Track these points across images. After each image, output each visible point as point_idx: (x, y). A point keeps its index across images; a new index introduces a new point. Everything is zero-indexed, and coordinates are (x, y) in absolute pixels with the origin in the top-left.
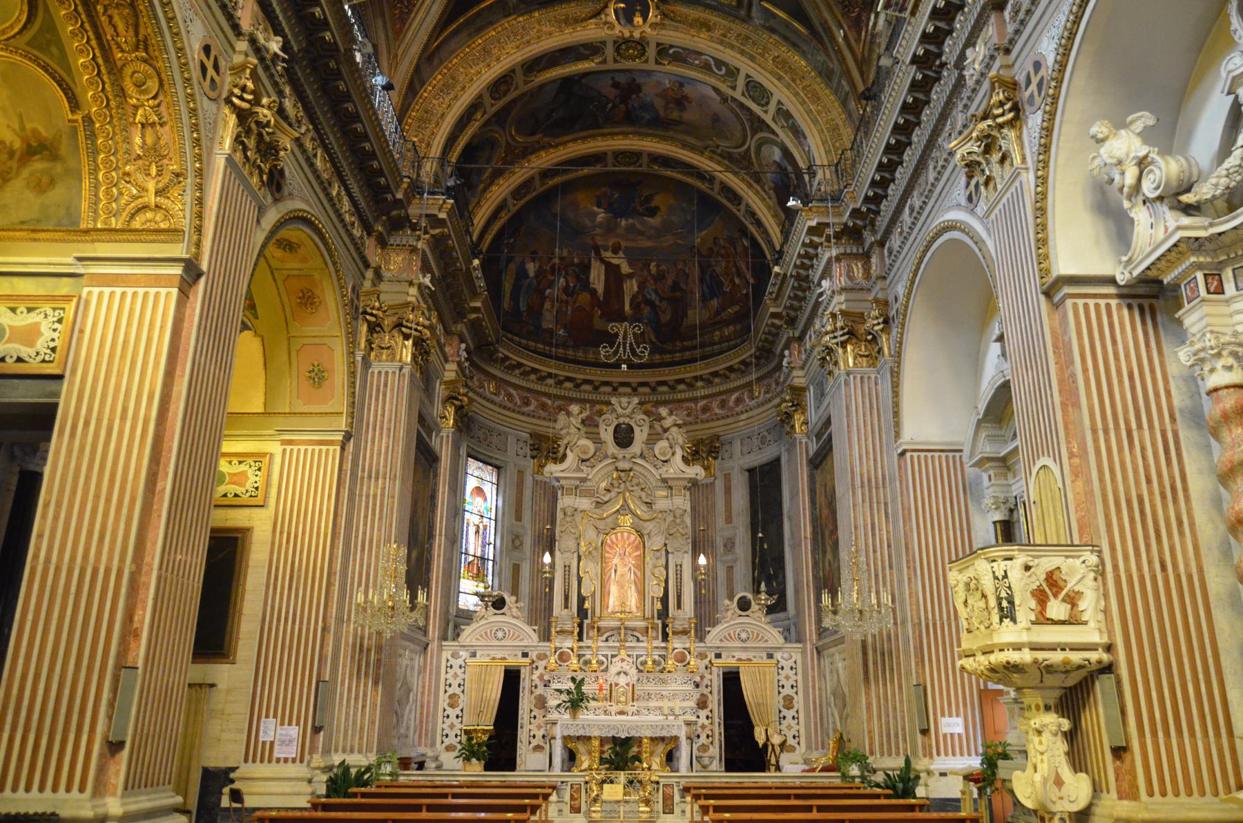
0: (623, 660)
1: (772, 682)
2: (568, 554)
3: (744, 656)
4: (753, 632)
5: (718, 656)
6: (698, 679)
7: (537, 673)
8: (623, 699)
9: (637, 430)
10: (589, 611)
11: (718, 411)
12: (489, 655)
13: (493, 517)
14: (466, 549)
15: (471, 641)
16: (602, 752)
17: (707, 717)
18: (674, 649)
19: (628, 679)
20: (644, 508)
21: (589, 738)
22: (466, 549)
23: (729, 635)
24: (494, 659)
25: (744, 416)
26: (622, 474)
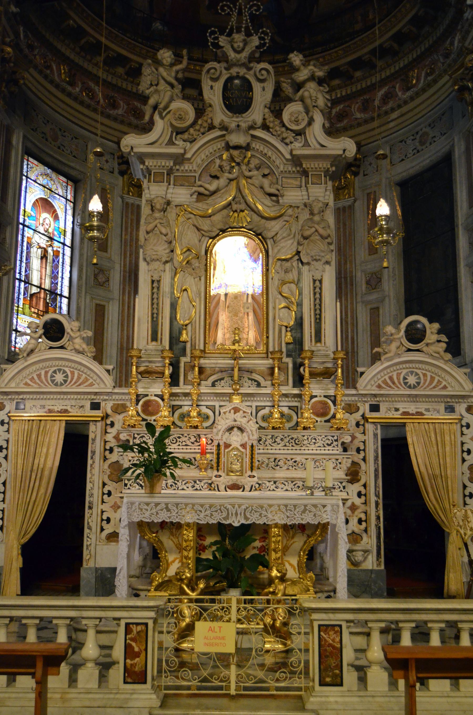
0: (236, 410)
1: (453, 445)
2: (156, 265)
3: (412, 408)
4: (425, 375)
5: (375, 408)
6: (348, 439)
7: (113, 431)
8: (237, 467)
9: (257, 87)
10: (188, 346)
11: (358, 115)
12: (44, 407)
13: (68, 242)
14: (27, 276)
15: (17, 386)
16: (201, 549)
17: (359, 495)
18: (312, 397)
19: (244, 438)
20: (268, 201)
21: (178, 526)
22: (27, 276)
23: (391, 378)
24: (50, 411)
25: (394, 115)
26: (235, 153)
